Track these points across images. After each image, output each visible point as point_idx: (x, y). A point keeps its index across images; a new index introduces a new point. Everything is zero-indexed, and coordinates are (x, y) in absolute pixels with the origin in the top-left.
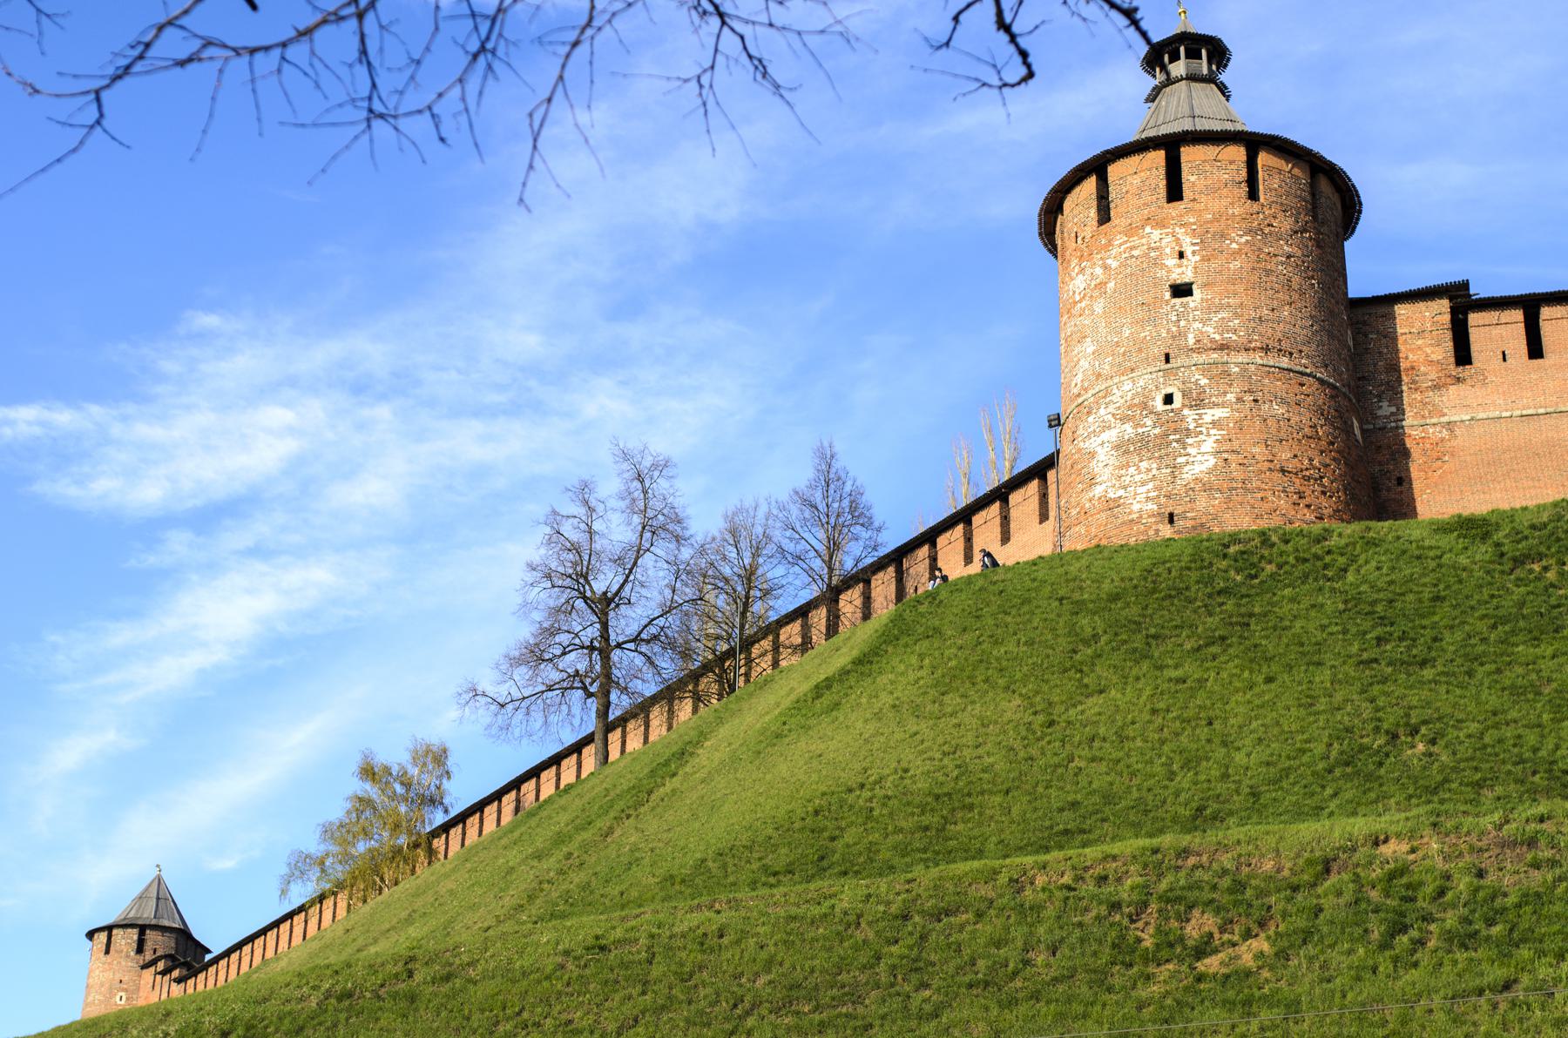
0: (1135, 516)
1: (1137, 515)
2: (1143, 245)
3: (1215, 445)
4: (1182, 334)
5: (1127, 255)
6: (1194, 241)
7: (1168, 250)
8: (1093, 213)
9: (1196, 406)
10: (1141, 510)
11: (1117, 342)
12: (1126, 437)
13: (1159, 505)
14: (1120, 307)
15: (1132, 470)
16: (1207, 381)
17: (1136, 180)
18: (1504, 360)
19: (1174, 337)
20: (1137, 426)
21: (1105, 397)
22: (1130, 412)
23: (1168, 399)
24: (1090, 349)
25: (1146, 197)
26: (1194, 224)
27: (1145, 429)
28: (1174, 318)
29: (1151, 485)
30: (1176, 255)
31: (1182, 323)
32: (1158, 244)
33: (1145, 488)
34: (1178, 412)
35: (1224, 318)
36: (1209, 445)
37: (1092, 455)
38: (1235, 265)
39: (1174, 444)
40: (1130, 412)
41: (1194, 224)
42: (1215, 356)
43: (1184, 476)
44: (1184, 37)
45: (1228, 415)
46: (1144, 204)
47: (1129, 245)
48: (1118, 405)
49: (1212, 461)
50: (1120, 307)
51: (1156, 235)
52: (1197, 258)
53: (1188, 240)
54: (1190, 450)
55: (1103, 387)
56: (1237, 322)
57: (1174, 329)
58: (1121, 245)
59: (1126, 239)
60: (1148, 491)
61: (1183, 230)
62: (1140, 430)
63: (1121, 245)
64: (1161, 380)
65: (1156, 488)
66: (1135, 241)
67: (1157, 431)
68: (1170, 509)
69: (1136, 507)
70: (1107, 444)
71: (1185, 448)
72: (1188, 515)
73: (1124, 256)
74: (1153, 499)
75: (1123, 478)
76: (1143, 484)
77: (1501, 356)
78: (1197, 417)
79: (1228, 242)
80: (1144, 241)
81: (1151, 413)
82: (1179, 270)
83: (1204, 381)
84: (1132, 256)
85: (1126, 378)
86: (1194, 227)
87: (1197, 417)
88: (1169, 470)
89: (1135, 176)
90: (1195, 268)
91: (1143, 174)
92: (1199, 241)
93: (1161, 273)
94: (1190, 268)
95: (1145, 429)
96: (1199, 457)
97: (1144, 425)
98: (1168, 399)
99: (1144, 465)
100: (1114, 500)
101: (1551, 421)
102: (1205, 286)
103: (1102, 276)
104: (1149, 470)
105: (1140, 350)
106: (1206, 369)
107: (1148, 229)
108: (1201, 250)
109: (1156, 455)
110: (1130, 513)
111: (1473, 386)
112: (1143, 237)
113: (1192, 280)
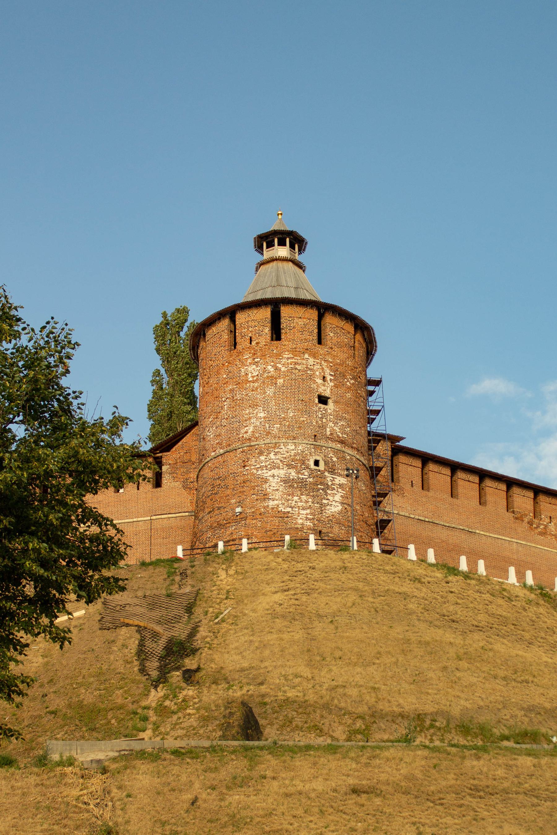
0: (299, 526)
1: (301, 526)
2: (303, 364)
3: (341, 498)
4: (323, 427)
5: (292, 366)
6: (331, 373)
7: (317, 373)
8: (267, 330)
9: (331, 472)
10: (302, 524)
11: (284, 417)
12: (291, 477)
13: (314, 524)
14: (287, 397)
15: (296, 498)
16: (336, 460)
17: (301, 322)
18: (412, 486)
19: (319, 427)
20: (298, 473)
21: (274, 448)
22: (293, 463)
23: (317, 463)
24: (262, 415)
25: (306, 335)
26: (331, 362)
27: (303, 476)
28: (320, 416)
29: (308, 511)
30: (322, 378)
31: (324, 420)
32: (312, 367)
33: (305, 512)
34: (323, 472)
35: (343, 425)
36: (338, 498)
37: (266, 481)
38: (349, 395)
39: (321, 491)
40: (293, 463)
41: (331, 362)
42: (339, 446)
43: (327, 511)
44: (275, 233)
45: (346, 483)
46: (305, 339)
47: (293, 360)
48: (284, 456)
49: (340, 508)
50: (287, 397)
51: (311, 361)
52: (332, 384)
53: (328, 371)
54: (329, 497)
55: (274, 441)
56: (349, 429)
57: (320, 422)
58: (288, 359)
59: (292, 356)
60: (307, 514)
61: (326, 364)
62: (301, 476)
63: (288, 359)
64: (313, 450)
65: (311, 514)
66: (298, 359)
67: (311, 480)
68: (320, 528)
69: (300, 521)
70: (276, 478)
71: (327, 496)
72: (330, 535)
73: (290, 366)
74: (310, 519)
75: (290, 502)
76: (304, 509)
77: (410, 484)
78: (332, 479)
79: (346, 380)
80: (304, 362)
81: (308, 468)
82: (323, 388)
83: (335, 459)
84: (296, 369)
85: (291, 441)
86: (331, 365)
87: (332, 479)
88: (318, 505)
89: (300, 320)
90: (331, 390)
91: (305, 320)
92: (333, 374)
93: (314, 386)
94: (329, 388)
95: (303, 476)
96: (334, 503)
97: (303, 474)
98: (317, 463)
99: (304, 498)
100: (284, 513)
101: (430, 526)
102: (335, 402)
103: (273, 373)
104: (307, 502)
105: (300, 428)
106: (336, 452)
107: (306, 356)
108: (334, 380)
109: (311, 494)
110: (295, 524)
111: (398, 496)
112: (303, 359)
113: (330, 396)
